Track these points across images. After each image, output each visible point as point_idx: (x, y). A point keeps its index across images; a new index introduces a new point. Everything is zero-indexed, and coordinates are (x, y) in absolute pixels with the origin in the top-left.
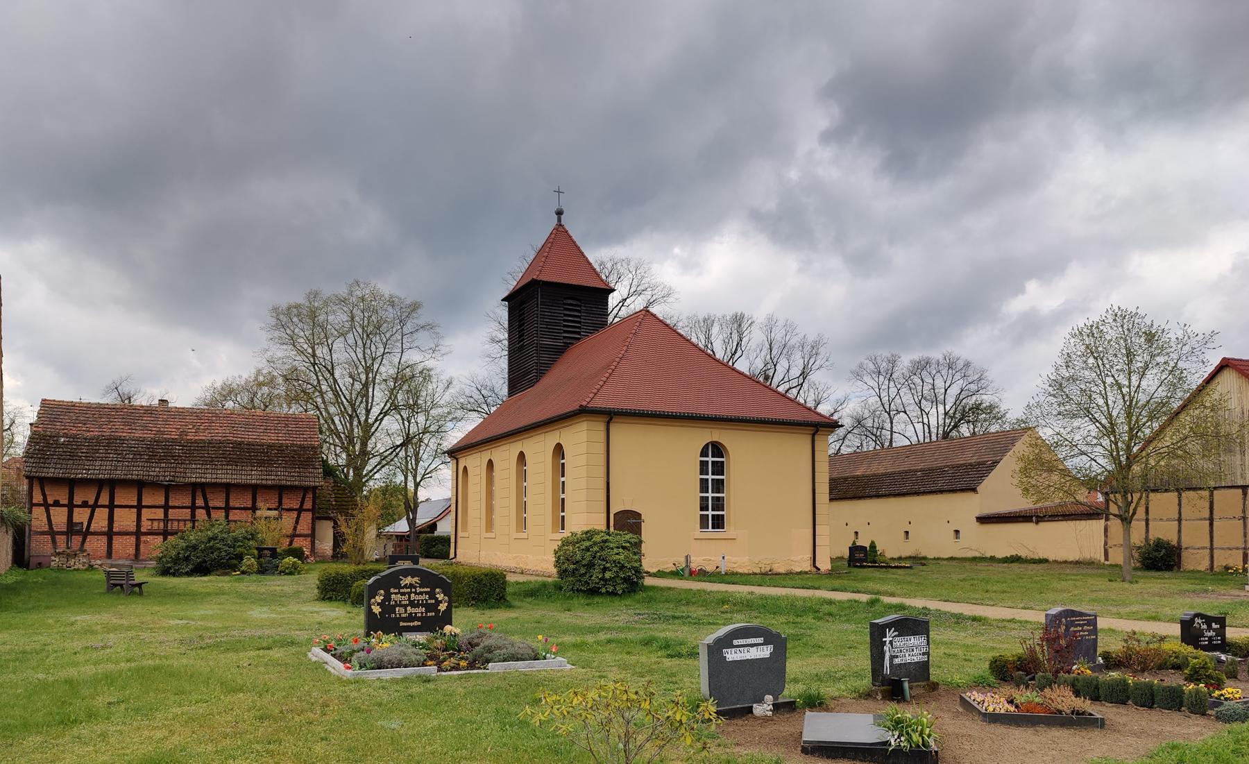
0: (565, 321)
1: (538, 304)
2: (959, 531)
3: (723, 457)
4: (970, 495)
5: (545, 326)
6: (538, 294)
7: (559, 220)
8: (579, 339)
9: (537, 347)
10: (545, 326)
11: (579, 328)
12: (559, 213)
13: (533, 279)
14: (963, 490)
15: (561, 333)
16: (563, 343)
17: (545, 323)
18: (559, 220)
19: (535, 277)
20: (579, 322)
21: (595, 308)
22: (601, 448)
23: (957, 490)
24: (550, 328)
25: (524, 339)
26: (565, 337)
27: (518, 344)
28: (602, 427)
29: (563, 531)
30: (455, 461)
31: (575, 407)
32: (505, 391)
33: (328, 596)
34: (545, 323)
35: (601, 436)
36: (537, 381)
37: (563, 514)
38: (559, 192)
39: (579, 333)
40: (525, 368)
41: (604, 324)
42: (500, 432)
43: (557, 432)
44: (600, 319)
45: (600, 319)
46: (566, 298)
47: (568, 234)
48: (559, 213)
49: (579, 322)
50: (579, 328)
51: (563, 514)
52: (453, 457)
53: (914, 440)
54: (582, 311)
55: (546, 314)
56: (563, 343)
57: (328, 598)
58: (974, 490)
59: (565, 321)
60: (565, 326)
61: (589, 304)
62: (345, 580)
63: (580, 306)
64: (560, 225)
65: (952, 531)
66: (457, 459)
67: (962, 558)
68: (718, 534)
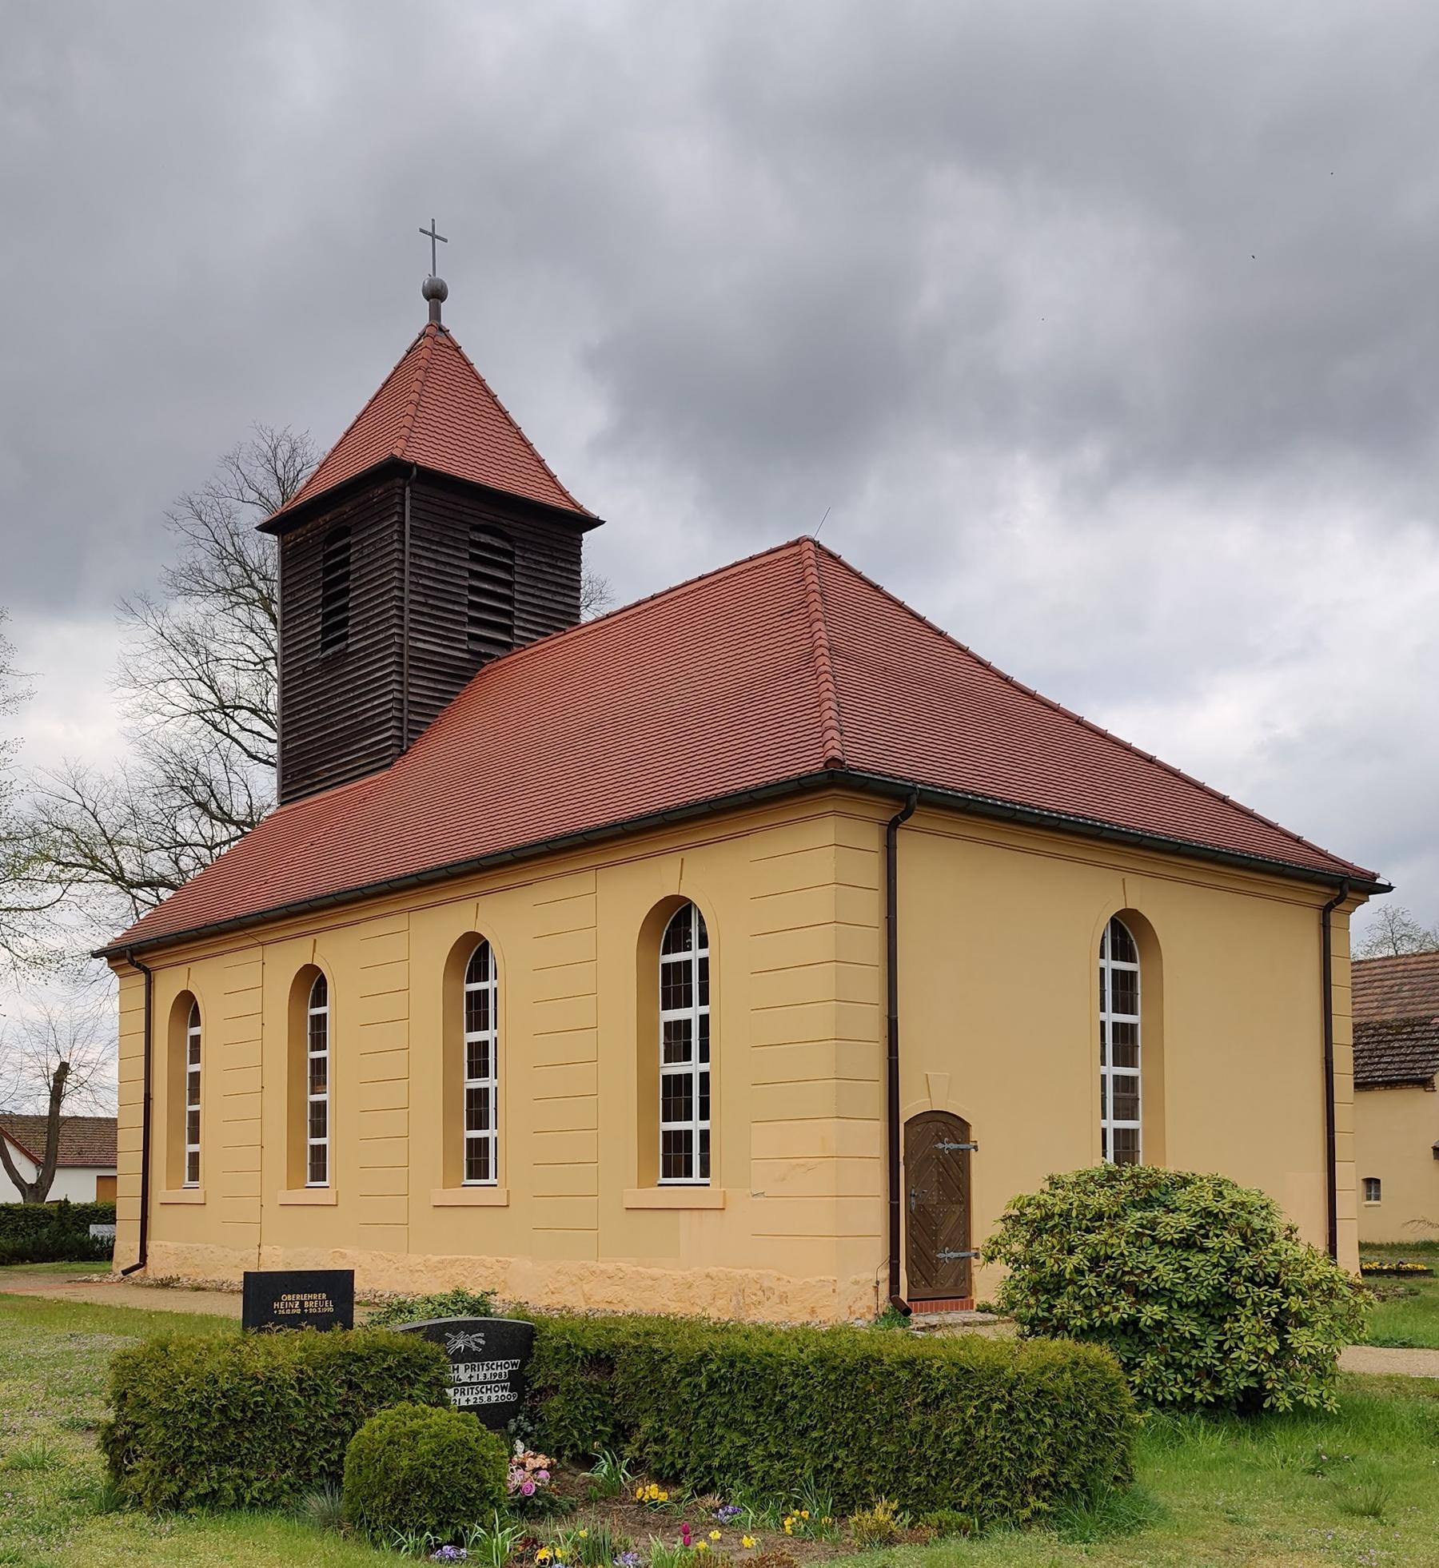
0: (474, 590)
1: (402, 533)
2: (1378, 1181)
3: (1133, 960)
4: (1416, 1095)
5: (421, 599)
6: (403, 505)
7: (435, 314)
8: (507, 646)
9: (401, 655)
10: (421, 599)
11: (508, 614)
12: (436, 294)
13: (393, 456)
14: (1390, 1084)
15: (463, 624)
16: (468, 651)
17: (421, 589)
18: (435, 314)
19: (397, 453)
20: (509, 600)
21: (550, 565)
22: (872, 907)
23: (1377, 1084)
24: (433, 607)
25: (345, 636)
26: (472, 637)
27: (323, 650)
28: (872, 838)
29: (194, 1184)
30: (141, 979)
31: (809, 763)
32: (265, 784)
33: (203, 1487)
34: (421, 589)
35: (871, 869)
36: (403, 753)
37: (194, 1148)
38: (433, 235)
39: (507, 630)
40: (356, 715)
41: (569, 616)
42: (603, 819)
43: (470, 905)
44: (560, 599)
45: (560, 599)
46: (476, 528)
47: (463, 357)
48: (436, 294)
49: (509, 600)
50: (508, 614)
51: (194, 1148)
52: (138, 966)
53: (69, 1077)
54: (517, 569)
55: (425, 563)
56: (468, 651)
57: (201, 1500)
58: (1425, 1083)
59: (474, 590)
60: (472, 605)
61: (533, 552)
62: (279, 1404)
63: (510, 555)
64: (441, 329)
65: (1361, 1182)
66: (148, 972)
67: (1400, 1245)
68: (475, 1193)
